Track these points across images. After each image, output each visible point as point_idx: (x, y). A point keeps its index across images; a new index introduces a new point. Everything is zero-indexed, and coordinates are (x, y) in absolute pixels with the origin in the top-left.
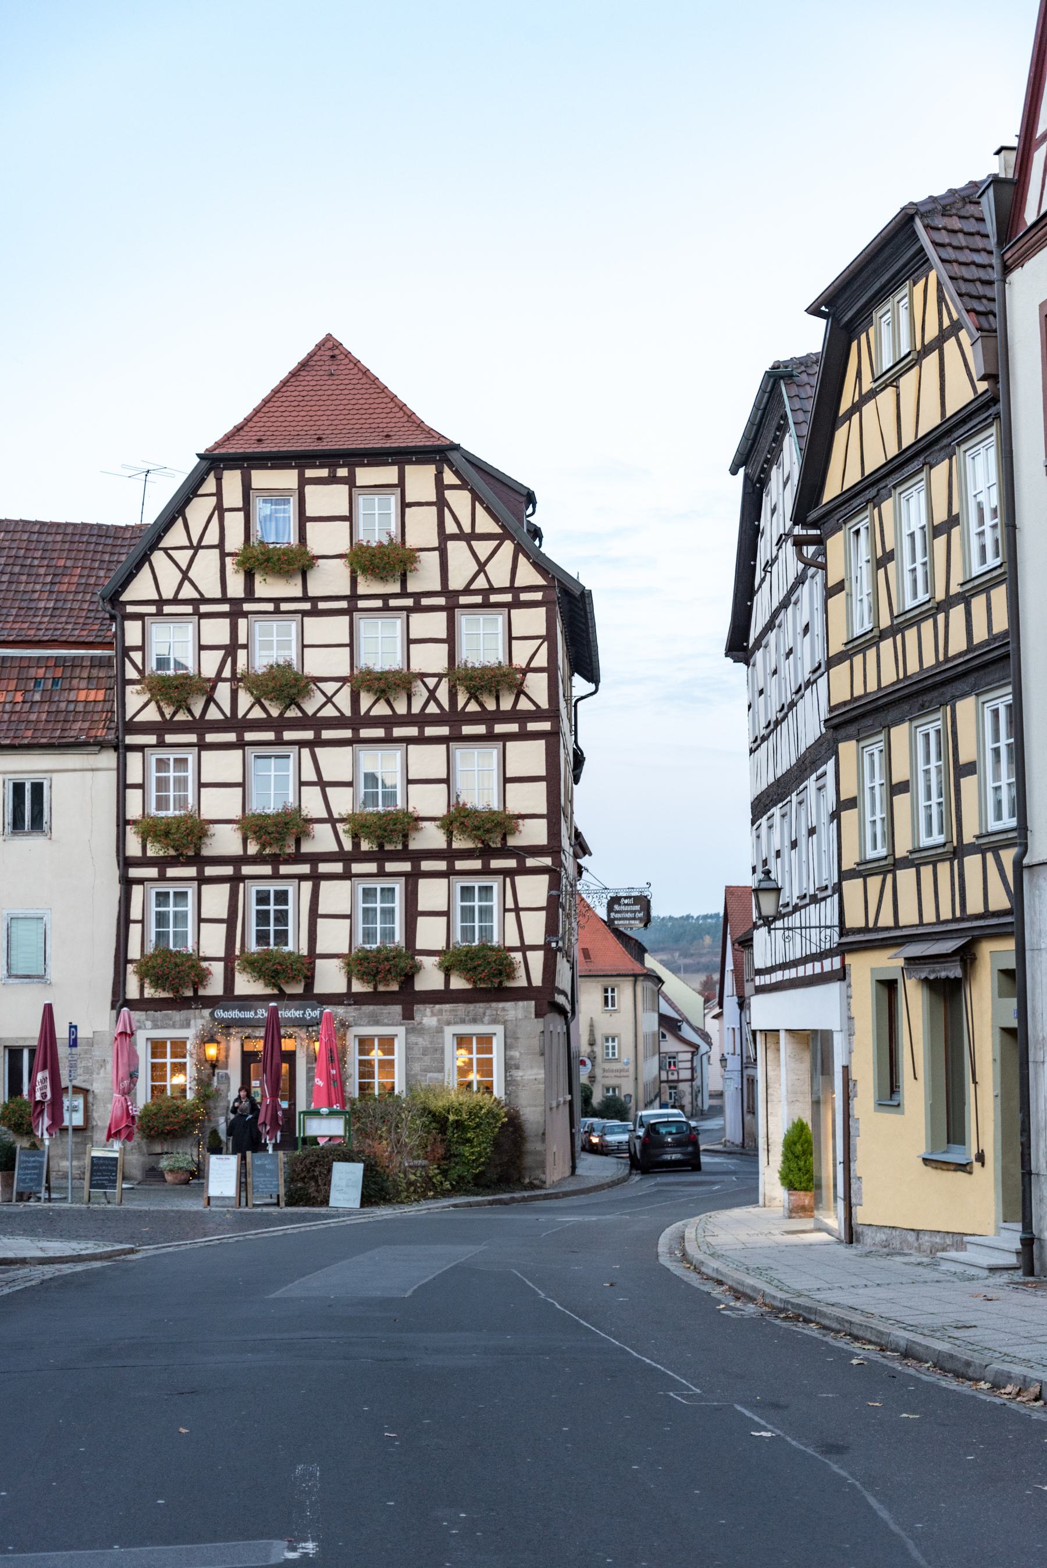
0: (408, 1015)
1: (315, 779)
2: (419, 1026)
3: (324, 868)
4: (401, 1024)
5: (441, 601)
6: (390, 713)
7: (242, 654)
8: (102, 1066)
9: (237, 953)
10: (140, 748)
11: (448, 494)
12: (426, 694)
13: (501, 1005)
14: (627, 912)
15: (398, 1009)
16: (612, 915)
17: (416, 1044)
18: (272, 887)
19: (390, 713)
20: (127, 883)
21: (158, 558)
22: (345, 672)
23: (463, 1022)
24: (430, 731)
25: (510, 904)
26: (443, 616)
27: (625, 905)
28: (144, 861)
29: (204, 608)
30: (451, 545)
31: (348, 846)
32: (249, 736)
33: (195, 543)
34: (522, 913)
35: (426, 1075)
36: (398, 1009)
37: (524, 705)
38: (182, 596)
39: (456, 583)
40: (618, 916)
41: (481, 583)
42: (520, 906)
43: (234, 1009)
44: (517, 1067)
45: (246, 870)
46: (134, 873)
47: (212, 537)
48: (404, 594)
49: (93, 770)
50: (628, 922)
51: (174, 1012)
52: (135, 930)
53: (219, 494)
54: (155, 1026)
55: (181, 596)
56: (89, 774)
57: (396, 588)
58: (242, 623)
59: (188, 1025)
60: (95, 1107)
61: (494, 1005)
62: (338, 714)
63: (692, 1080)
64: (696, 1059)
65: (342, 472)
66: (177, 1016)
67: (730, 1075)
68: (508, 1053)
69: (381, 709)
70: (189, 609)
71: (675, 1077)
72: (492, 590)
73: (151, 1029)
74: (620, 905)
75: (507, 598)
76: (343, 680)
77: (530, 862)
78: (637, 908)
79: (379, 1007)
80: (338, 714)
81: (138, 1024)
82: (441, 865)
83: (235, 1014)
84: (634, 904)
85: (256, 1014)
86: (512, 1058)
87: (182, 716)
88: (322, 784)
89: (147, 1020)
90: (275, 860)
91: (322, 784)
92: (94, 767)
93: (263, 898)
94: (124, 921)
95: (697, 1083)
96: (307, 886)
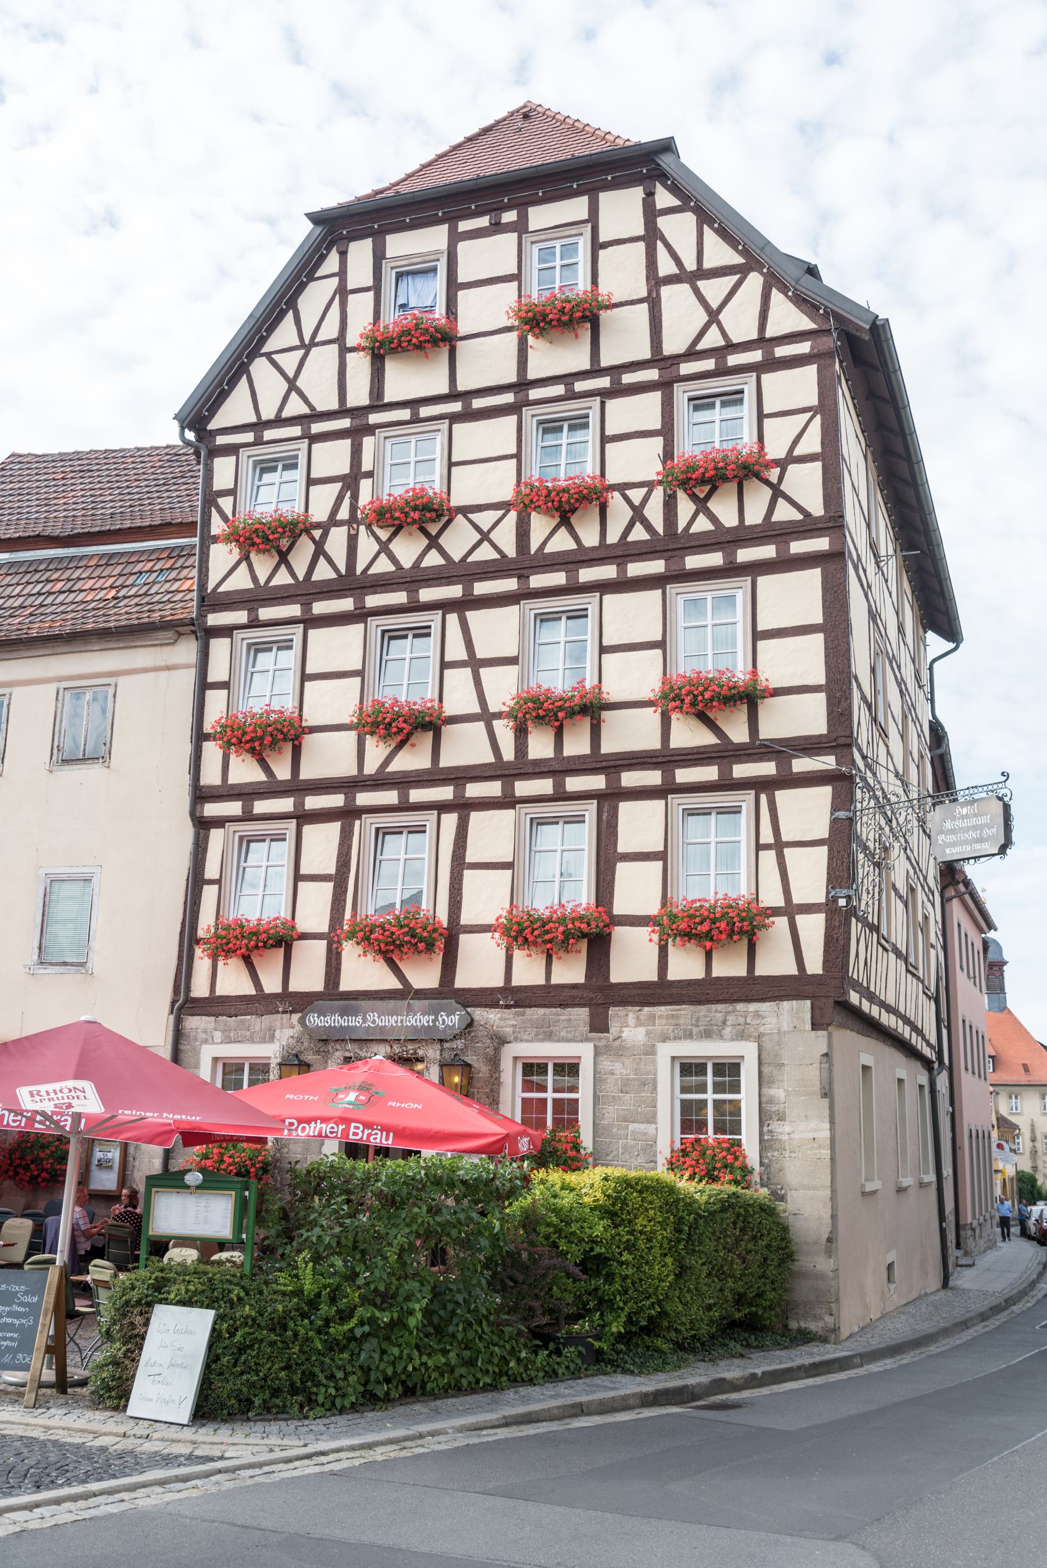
3: (474, 790)
11: (662, 222)
13: (753, 1007)
14: (967, 830)
15: (581, 1014)
20: (203, 825)
21: (260, 368)
23: (689, 1036)
29: (317, 428)
40: (953, 838)
43: (333, 1013)
45: (364, 799)
46: (211, 810)
49: (168, 668)
53: (342, 273)
54: (228, 1040)
56: (164, 674)
58: (368, 442)
59: (272, 1039)
61: (740, 1006)
62: (497, 556)
65: (510, 216)
76: (504, 506)
77: (801, 765)
81: (204, 1036)
82: (653, 778)
85: (365, 1020)
91: (475, 663)
92: (169, 663)
94: (197, 881)
96: (450, 820)
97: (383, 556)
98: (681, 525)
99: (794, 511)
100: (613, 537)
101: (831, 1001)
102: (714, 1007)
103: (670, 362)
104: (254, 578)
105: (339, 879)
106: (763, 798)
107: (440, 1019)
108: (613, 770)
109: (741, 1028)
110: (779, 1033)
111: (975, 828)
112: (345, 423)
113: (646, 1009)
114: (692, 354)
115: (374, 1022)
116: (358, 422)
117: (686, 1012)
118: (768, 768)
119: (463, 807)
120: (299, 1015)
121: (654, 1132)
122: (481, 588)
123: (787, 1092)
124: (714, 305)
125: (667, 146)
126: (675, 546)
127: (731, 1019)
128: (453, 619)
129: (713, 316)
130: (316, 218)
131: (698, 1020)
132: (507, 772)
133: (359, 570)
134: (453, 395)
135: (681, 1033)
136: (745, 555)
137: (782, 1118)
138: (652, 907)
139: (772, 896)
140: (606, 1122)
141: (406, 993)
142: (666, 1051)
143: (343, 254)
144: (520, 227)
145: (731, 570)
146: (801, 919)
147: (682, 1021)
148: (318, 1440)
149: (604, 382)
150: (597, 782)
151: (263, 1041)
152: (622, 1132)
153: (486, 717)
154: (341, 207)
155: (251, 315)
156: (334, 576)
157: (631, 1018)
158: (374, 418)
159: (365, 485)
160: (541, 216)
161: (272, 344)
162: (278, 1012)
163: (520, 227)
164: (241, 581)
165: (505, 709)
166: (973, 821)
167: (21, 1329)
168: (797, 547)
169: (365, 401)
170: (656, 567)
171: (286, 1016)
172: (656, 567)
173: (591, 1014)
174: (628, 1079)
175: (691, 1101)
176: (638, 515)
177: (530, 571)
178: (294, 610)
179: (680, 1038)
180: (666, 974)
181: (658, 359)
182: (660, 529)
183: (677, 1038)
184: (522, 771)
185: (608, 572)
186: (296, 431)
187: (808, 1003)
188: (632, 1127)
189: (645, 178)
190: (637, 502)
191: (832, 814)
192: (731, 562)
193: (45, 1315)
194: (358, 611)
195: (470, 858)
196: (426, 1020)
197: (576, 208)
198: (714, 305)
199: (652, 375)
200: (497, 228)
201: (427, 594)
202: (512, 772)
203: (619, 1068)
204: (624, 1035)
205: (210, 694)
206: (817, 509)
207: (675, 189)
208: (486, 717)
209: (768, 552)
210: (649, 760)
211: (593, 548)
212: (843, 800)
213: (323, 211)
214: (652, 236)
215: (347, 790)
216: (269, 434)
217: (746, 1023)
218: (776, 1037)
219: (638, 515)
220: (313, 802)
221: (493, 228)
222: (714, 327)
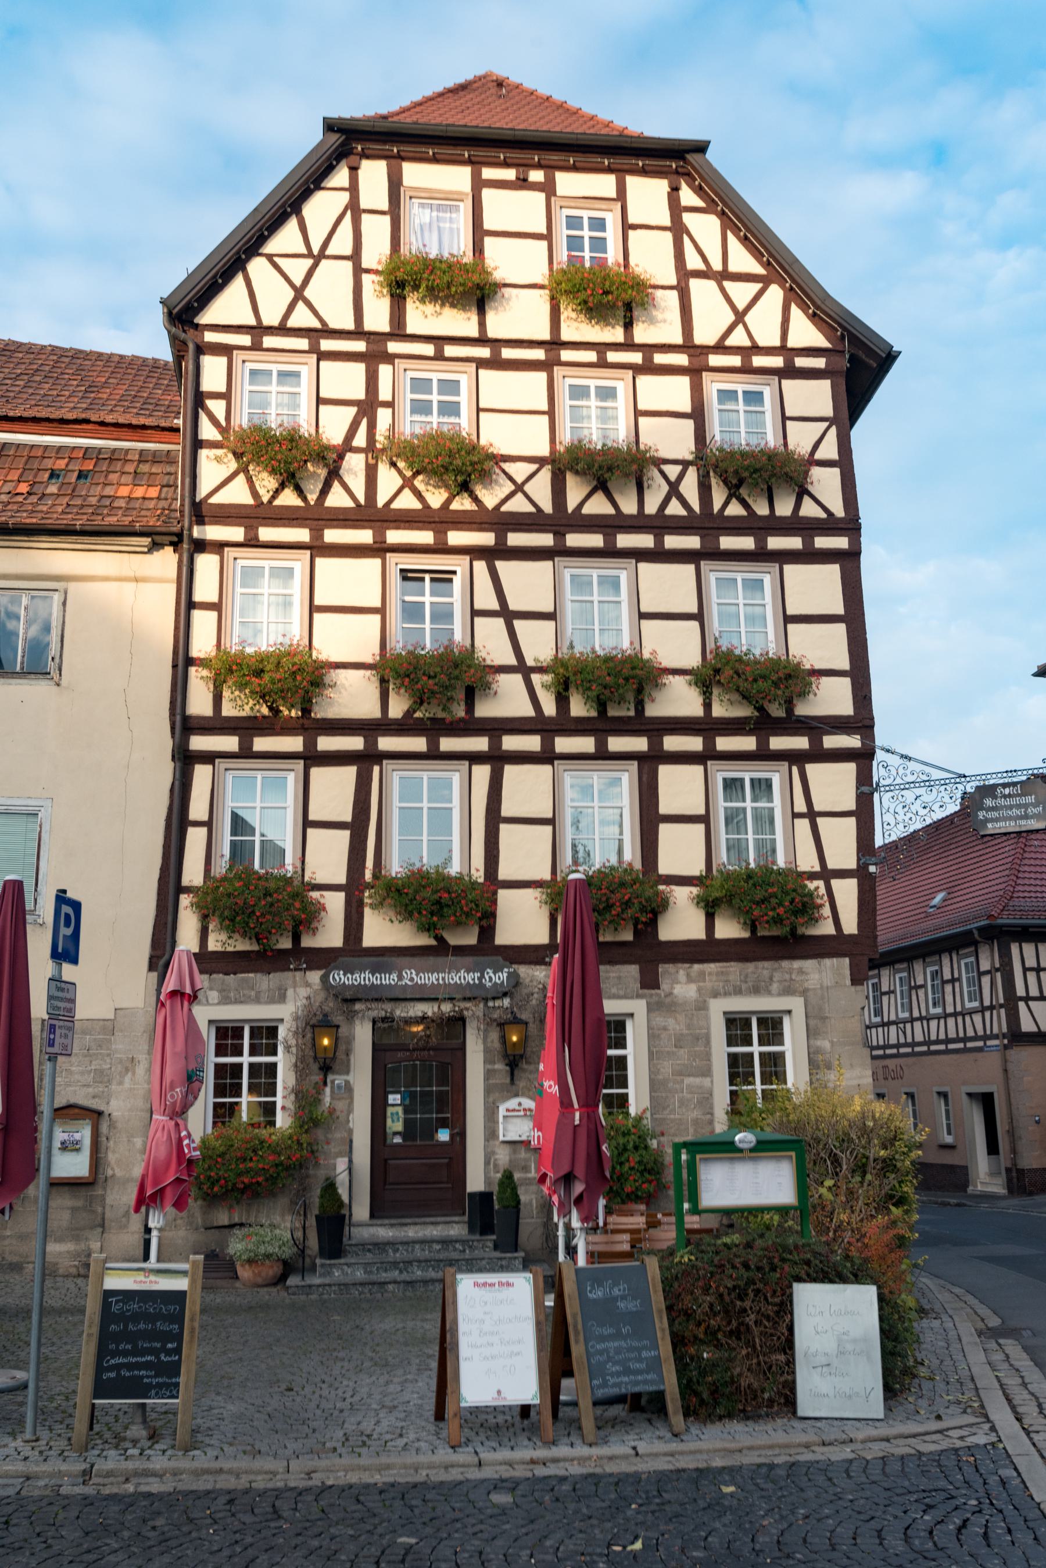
3: (511, 743)
6: (611, 511)
8: (127, 1070)
9: (368, 876)
11: (687, 218)
13: (797, 964)
14: (1011, 807)
15: (632, 971)
17: (665, 1029)
19: (611, 511)
21: (257, 266)
22: (544, 451)
23: (738, 992)
25: (801, 806)
27: (1005, 796)
29: (326, 345)
31: (550, 708)
37: (809, 509)
38: (292, 323)
40: (994, 814)
43: (362, 969)
45: (386, 743)
46: (199, 743)
47: (342, 243)
48: (628, 345)
49: (136, 580)
51: (259, 975)
53: (353, 189)
54: (225, 1000)
56: (133, 585)
57: (617, 334)
58: (385, 371)
59: (282, 999)
61: (785, 964)
62: (532, 509)
65: (536, 176)
66: (263, 982)
72: (756, 349)
73: (219, 1004)
74: (995, 797)
76: (541, 461)
77: (831, 742)
80: (532, 509)
82: (694, 743)
85: (400, 977)
87: (289, 498)
90: (434, 729)
91: (508, 615)
92: (139, 574)
96: (482, 773)
97: (407, 491)
98: (571, 506)
99: (819, 509)
100: (651, 507)
101: (866, 959)
102: (760, 964)
103: (699, 351)
104: (255, 494)
105: (357, 827)
106: (795, 769)
107: (487, 977)
108: (656, 733)
109: (787, 984)
110: (822, 987)
111: (1019, 806)
112: (360, 346)
114: (720, 348)
115: (412, 979)
116: (374, 347)
117: (734, 969)
118: (801, 743)
119: (497, 759)
120: (320, 973)
121: (709, 1084)
122: (515, 539)
123: (832, 1042)
124: (741, 306)
125: (701, 148)
126: (711, 525)
127: (777, 976)
128: (480, 566)
129: (740, 317)
130: (331, 126)
131: (746, 976)
132: (548, 727)
133: (381, 502)
134: (482, 340)
135: (731, 989)
136: (775, 543)
137: (829, 1067)
138: (696, 867)
139: (808, 862)
140: (661, 1077)
141: (442, 948)
142: (718, 1008)
143: (354, 169)
144: (548, 188)
145: (761, 555)
146: (835, 883)
147: (731, 977)
148: (908, 1419)
149: (636, 358)
150: (639, 744)
151: (271, 1001)
152: (677, 1086)
153: (522, 668)
154: (352, 119)
155: (256, 209)
156: (351, 504)
157: (682, 975)
158: (393, 347)
159: (384, 416)
160: (568, 183)
161: (272, 246)
162: (289, 970)
163: (548, 188)
164: (237, 494)
165: (790, 657)
166: (1017, 800)
167: (115, 1354)
168: (822, 542)
169: (386, 328)
170: (692, 542)
171: (298, 974)
172: (692, 542)
173: (641, 972)
174: (682, 1035)
175: (225, 1065)
176: (674, 490)
177: (568, 529)
178: (302, 535)
179: (730, 994)
180: (713, 933)
181: (688, 346)
182: (696, 507)
183: (726, 994)
184: (564, 727)
185: (645, 541)
186: (303, 344)
187: (847, 961)
188: (688, 1080)
189: (671, 173)
190: (673, 478)
191: (857, 788)
192: (762, 548)
193: (661, 1318)
194: (377, 545)
195: (506, 811)
196: (472, 978)
197: (604, 184)
198: (741, 307)
199: (681, 359)
200: (522, 183)
201: (456, 538)
202: (554, 727)
203: (674, 1024)
204: (676, 991)
205: (197, 615)
206: (839, 511)
207: (699, 191)
208: (522, 668)
209: (795, 543)
210: (693, 726)
211: (631, 516)
212: (864, 778)
213: (340, 119)
214: (678, 230)
215: (367, 733)
216: (268, 341)
217: (791, 979)
218: (819, 992)
219: (674, 490)
220: (326, 743)
221: (520, 183)
222: (740, 327)
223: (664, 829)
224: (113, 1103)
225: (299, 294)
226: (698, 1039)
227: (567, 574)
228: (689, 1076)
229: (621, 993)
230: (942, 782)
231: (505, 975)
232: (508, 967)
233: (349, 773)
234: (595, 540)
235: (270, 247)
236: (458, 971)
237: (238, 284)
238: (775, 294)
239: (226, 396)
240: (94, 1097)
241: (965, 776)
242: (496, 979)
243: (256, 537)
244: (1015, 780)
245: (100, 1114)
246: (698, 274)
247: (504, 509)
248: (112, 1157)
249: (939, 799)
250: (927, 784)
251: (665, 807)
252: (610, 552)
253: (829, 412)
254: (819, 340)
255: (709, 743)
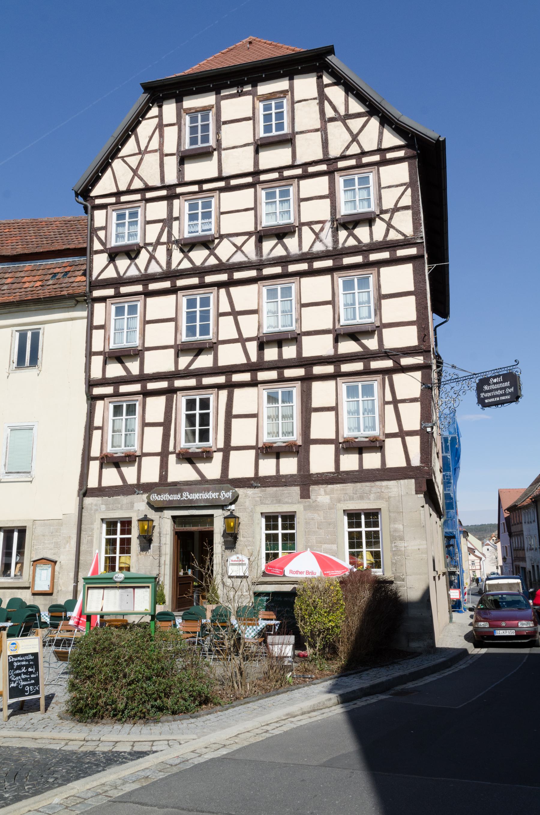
0: (305, 495)
1: (229, 309)
2: (314, 504)
3: (237, 378)
4: (299, 502)
5: (323, 167)
7: (175, 224)
8: (67, 542)
10: (103, 299)
11: (328, 91)
12: (385, 226)
13: (385, 483)
14: (497, 390)
15: (296, 490)
16: (482, 395)
17: (313, 519)
18: (198, 396)
20: (92, 399)
21: (117, 164)
22: (252, 228)
23: (351, 499)
24: (317, 265)
25: (388, 397)
26: (325, 179)
27: (494, 384)
28: (104, 382)
29: (149, 195)
30: (331, 126)
32: (180, 283)
33: (143, 148)
34: (400, 406)
35: (321, 546)
36: (296, 490)
38: (133, 187)
39: (334, 151)
40: (489, 394)
41: (354, 149)
42: (399, 397)
43: (165, 493)
44: (402, 539)
45: (179, 383)
47: (154, 144)
50: (498, 399)
52: (97, 435)
53: (160, 116)
55: (132, 188)
58: (176, 202)
60: (61, 575)
61: (378, 483)
63: (480, 569)
64: (481, 562)
65: (248, 88)
67: (507, 565)
68: (392, 526)
69: (279, 252)
70: (138, 197)
71: (474, 568)
72: (364, 153)
74: (489, 385)
75: (376, 158)
76: (249, 234)
77: (405, 361)
78: (507, 384)
79: (281, 488)
82: (330, 369)
83: (166, 497)
84: (504, 381)
85: (182, 496)
86: (396, 530)
88: (235, 313)
89: (102, 504)
91: (235, 313)
93: (191, 404)
94: (90, 428)
95: (482, 570)
107: (222, 495)
110: (399, 496)
111: (501, 389)
112: (164, 193)
113: (329, 486)
115: (187, 497)
116: (170, 192)
121: (336, 548)
170: (329, 263)
172: (329, 263)
174: (321, 522)
198: (355, 132)
200: (240, 94)
216: (123, 199)
223: (314, 415)
224: (62, 557)
225: (135, 172)
226: (330, 524)
227: (340, 282)
228: (325, 544)
229: (290, 501)
230: (464, 378)
231: (231, 493)
232: (232, 490)
233: (162, 400)
234: (278, 270)
235: (121, 154)
236: (208, 492)
237: (109, 173)
238: (374, 123)
239: (105, 228)
240: (54, 554)
241: (476, 374)
242: (226, 496)
243: (119, 292)
244: (500, 373)
245: (55, 562)
246: (332, 120)
247: (100, 278)
248: (61, 582)
249: (462, 388)
250: (457, 380)
251: (315, 404)
252: (285, 275)
253: (407, 179)
254: (399, 142)
255: (337, 368)
